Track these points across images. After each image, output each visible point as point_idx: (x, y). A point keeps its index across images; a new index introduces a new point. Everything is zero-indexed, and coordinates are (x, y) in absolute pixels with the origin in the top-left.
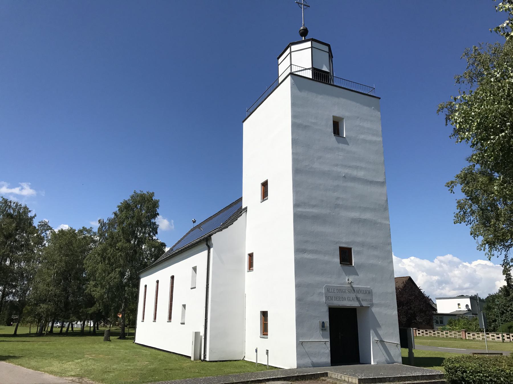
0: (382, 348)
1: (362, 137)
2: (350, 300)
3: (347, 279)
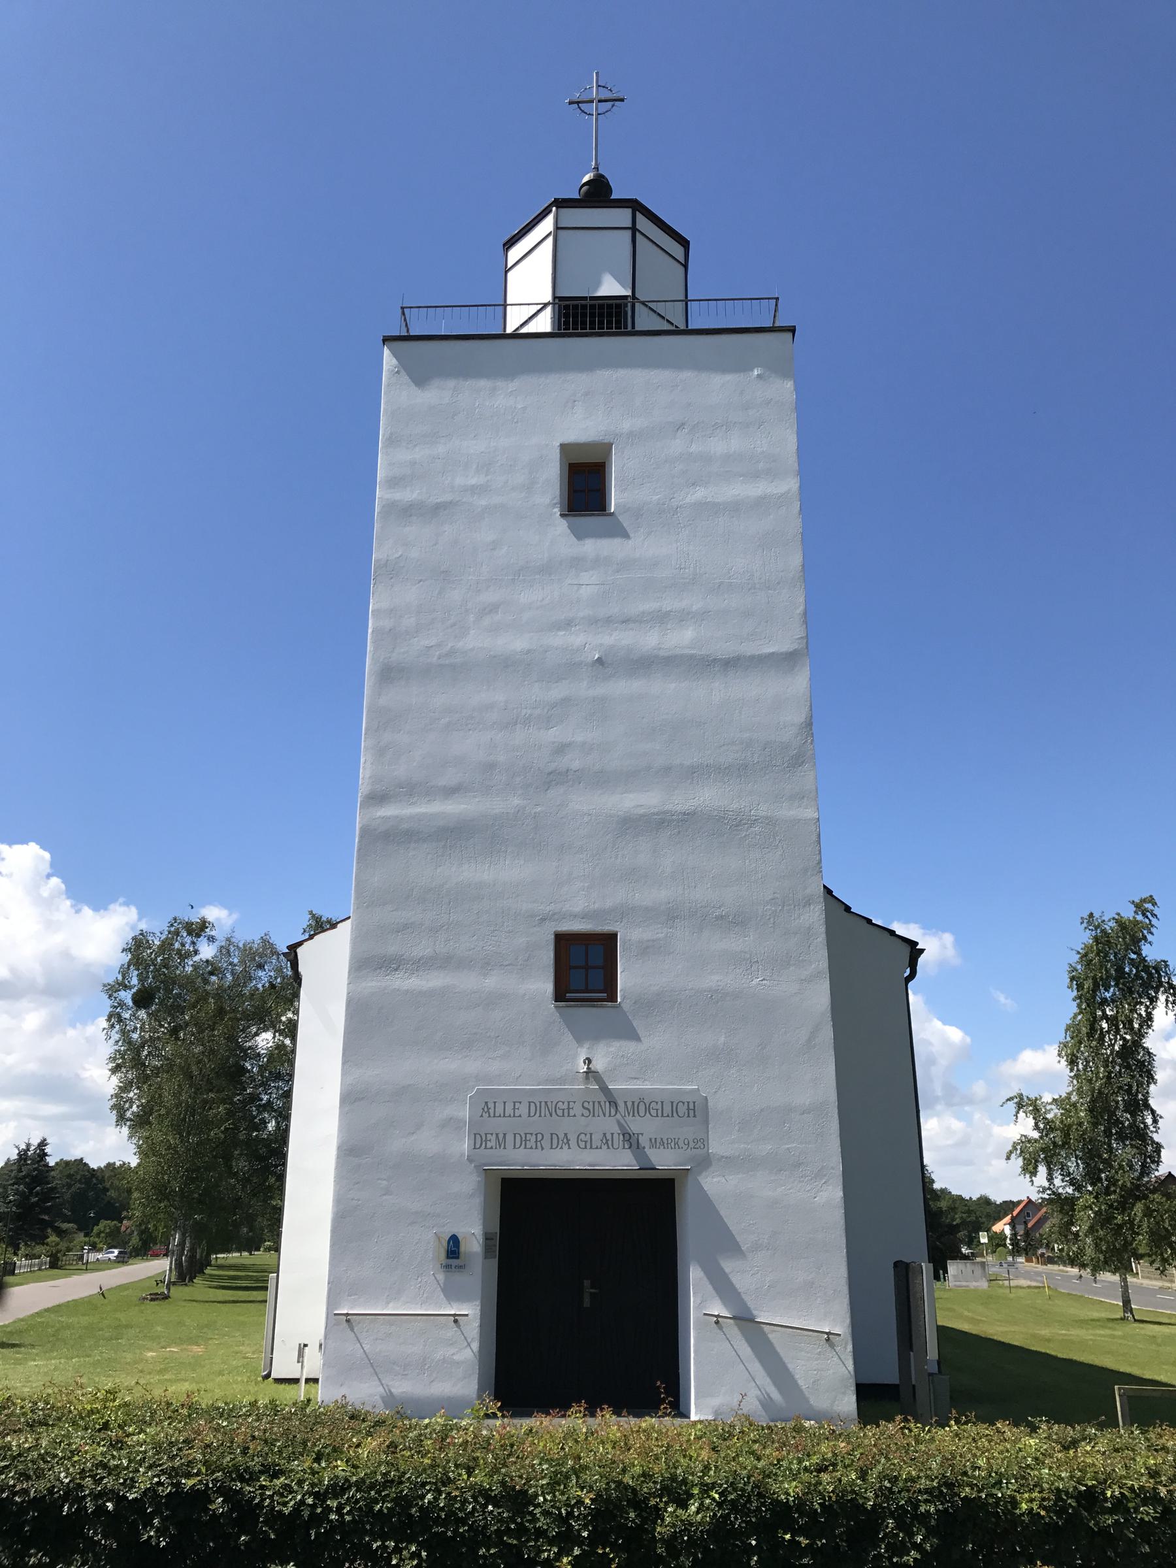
0: (745, 1350)
1: (700, 494)
2: (589, 1145)
3: (580, 1056)
